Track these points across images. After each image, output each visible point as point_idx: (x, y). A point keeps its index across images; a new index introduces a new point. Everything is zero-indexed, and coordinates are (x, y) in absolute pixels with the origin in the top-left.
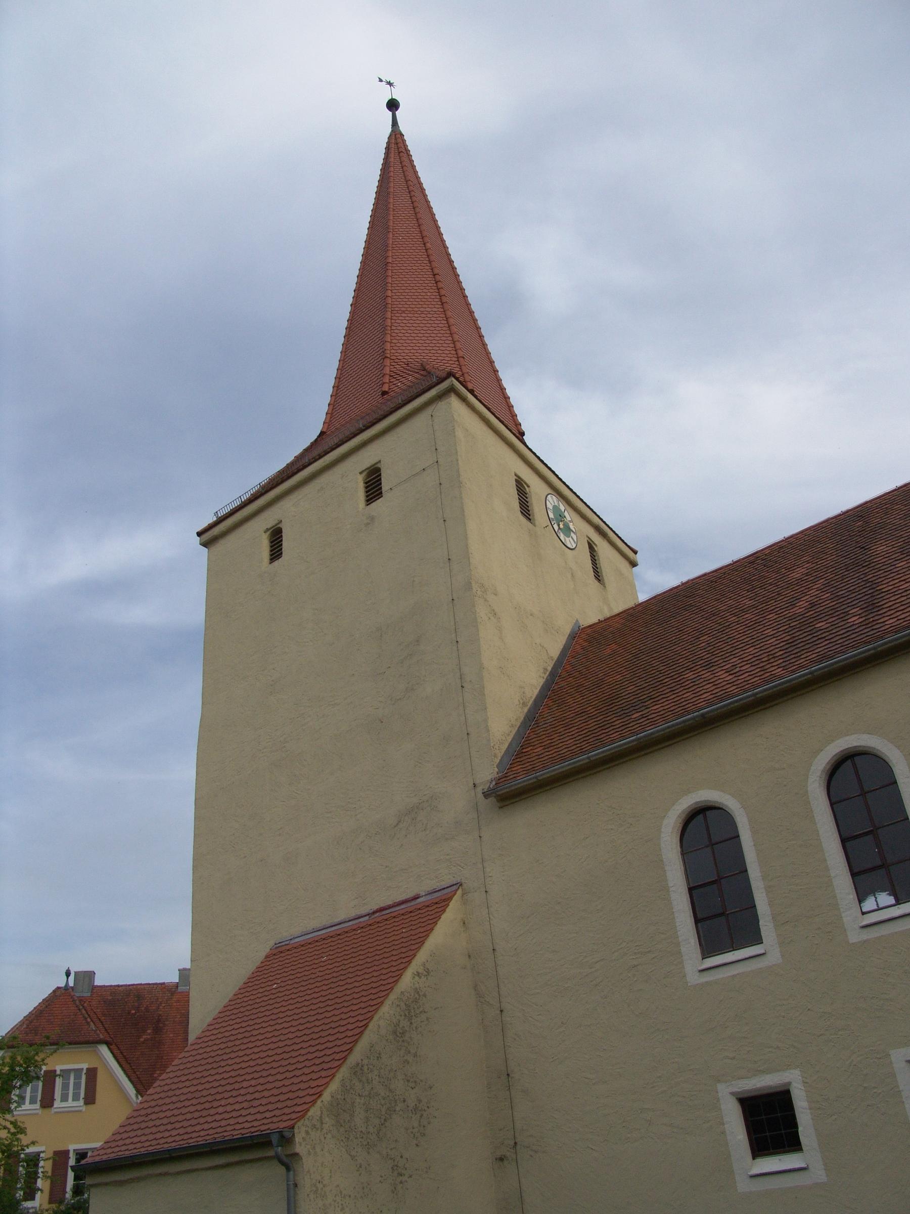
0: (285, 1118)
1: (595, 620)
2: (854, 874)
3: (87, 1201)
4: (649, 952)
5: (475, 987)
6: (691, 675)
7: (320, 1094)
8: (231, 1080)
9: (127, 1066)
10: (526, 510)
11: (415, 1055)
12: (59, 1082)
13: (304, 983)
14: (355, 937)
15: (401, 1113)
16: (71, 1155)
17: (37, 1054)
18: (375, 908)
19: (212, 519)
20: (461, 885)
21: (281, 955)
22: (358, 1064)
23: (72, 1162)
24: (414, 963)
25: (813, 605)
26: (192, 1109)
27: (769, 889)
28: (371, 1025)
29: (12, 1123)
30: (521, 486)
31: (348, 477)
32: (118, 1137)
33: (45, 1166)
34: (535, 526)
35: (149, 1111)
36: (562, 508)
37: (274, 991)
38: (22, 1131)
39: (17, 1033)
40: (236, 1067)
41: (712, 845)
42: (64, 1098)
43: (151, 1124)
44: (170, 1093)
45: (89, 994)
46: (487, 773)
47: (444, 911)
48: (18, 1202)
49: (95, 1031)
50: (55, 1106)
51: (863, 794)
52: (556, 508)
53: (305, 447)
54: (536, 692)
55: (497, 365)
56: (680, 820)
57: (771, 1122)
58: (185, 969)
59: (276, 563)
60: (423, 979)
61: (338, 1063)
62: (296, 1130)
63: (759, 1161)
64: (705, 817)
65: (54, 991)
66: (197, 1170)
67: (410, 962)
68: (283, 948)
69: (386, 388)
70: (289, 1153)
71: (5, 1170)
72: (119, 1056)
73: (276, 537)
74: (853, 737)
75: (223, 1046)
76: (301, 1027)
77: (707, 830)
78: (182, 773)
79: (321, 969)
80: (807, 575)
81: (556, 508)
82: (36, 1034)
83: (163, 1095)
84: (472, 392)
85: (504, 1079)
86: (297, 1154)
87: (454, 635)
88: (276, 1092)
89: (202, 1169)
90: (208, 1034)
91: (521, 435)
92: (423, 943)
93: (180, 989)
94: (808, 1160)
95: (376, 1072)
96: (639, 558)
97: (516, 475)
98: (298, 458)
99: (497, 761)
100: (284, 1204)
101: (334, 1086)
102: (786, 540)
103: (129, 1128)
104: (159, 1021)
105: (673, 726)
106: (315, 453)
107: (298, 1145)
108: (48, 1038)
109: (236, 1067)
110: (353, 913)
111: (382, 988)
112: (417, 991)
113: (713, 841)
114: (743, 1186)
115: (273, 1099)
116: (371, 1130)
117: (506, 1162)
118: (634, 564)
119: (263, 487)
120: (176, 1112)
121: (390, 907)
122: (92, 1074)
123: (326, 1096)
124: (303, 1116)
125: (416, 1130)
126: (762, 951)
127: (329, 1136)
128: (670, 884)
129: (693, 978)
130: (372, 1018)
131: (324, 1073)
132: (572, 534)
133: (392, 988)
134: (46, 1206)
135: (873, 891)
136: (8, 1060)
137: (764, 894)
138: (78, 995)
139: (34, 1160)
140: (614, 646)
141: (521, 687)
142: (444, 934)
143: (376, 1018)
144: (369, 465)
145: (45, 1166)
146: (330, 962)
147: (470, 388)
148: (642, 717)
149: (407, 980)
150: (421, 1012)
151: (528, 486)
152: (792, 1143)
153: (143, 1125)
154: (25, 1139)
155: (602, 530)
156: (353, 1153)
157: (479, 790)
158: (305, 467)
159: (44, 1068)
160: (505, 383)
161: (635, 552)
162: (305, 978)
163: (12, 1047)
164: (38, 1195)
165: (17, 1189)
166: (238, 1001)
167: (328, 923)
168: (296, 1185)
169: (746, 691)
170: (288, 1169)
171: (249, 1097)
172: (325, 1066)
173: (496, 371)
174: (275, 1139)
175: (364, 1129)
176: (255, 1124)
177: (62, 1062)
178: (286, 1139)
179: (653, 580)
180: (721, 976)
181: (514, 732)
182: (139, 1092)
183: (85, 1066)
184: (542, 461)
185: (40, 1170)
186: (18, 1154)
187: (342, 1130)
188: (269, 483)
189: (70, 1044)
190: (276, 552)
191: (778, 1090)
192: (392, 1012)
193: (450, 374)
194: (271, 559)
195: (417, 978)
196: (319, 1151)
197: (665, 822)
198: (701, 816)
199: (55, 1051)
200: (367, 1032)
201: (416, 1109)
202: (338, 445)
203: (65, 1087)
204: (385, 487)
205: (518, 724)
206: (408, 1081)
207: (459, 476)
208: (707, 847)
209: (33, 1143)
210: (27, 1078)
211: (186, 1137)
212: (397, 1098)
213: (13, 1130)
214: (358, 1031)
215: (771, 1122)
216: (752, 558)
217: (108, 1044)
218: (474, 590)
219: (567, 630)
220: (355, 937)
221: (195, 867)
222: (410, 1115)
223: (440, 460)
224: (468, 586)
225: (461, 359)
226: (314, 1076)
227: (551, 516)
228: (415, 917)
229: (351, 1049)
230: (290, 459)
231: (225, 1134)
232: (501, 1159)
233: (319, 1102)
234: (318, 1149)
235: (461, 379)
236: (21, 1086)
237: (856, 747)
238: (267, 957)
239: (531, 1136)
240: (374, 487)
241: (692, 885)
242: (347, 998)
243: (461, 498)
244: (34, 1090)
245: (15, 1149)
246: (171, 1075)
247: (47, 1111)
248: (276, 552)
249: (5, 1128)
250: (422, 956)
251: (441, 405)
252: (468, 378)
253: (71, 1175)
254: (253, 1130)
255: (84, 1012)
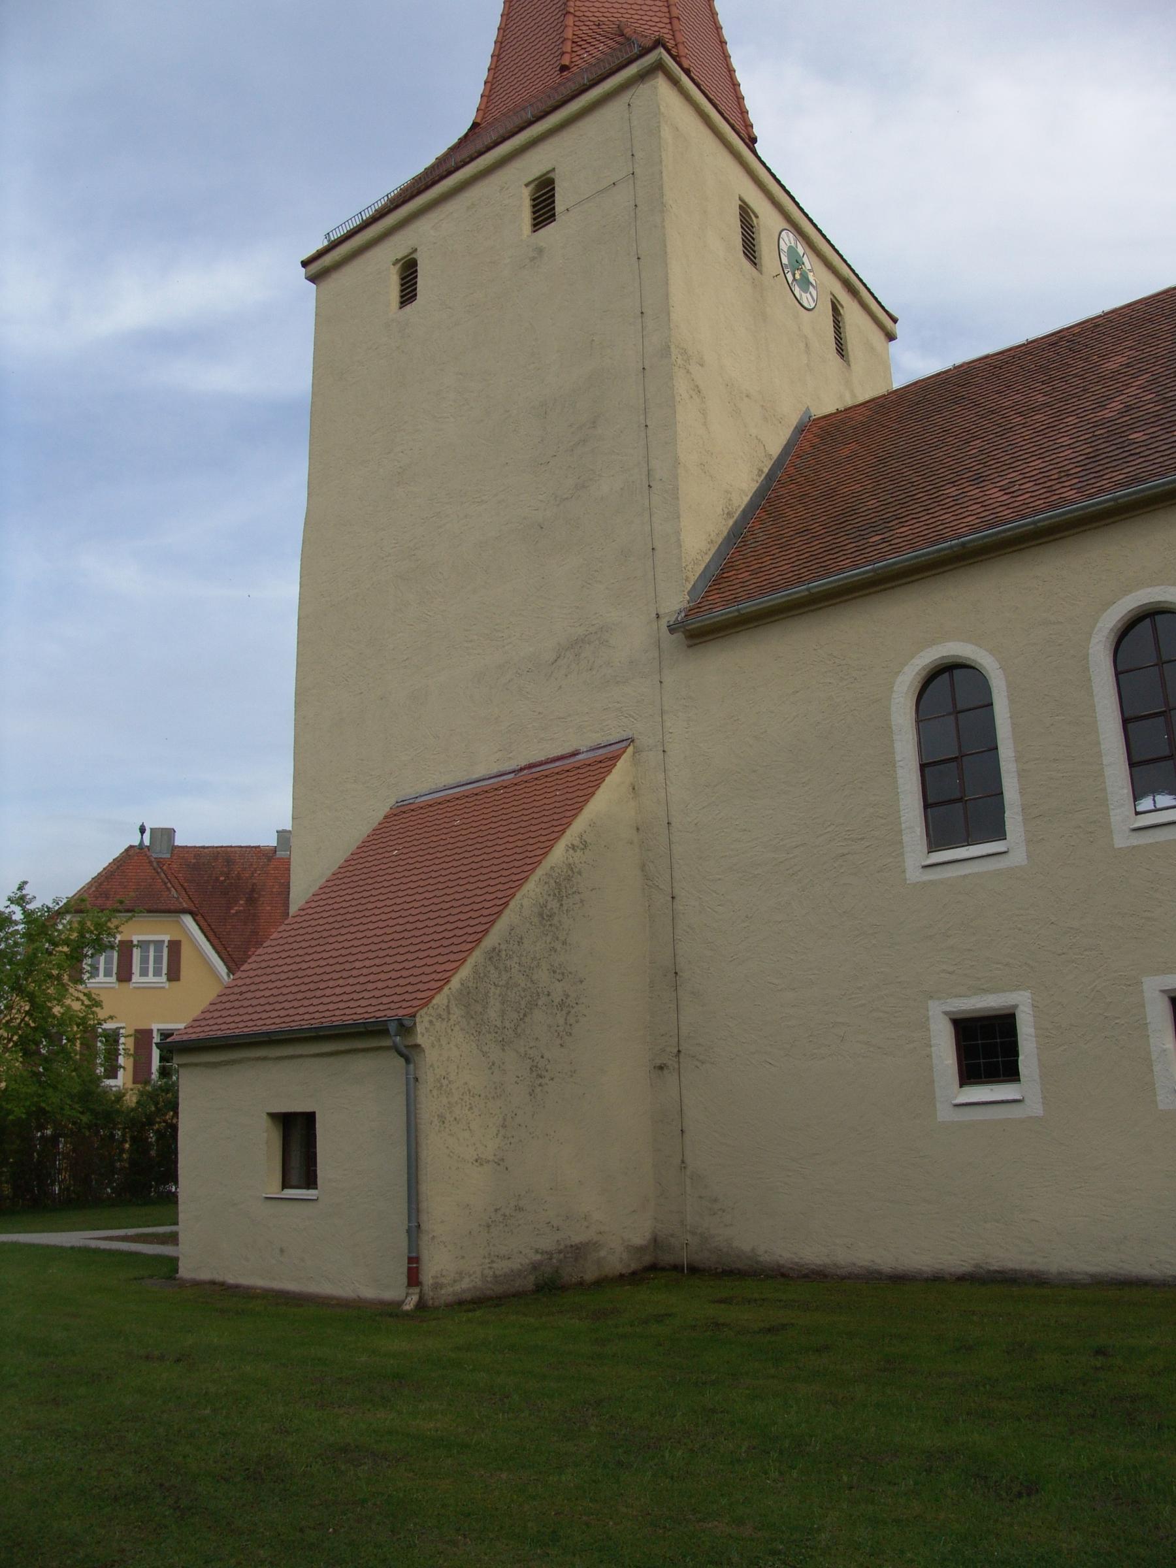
0: (405, 1004)
1: (831, 409)
2: (1132, 765)
3: (176, 1084)
4: (862, 839)
5: (643, 867)
6: (953, 491)
7: (447, 981)
8: (341, 960)
9: (216, 942)
10: (750, 250)
11: (564, 943)
12: (136, 953)
13: (431, 851)
14: (497, 798)
15: (544, 1008)
16: (155, 1034)
17: (110, 920)
18: (523, 764)
19: (322, 244)
20: (633, 741)
21: (404, 816)
22: (494, 949)
23: (156, 1039)
24: (568, 833)
25: (1129, 408)
26: (294, 989)
27: (1021, 774)
28: (512, 904)
29: (85, 994)
30: (746, 215)
31: (510, 190)
32: (208, 1015)
33: (126, 1043)
34: (761, 272)
35: (244, 989)
36: (800, 250)
37: (394, 859)
38: (98, 1004)
39: (86, 896)
40: (347, 944)
41: (957, 712)
42: (144, 972)
43: (246, 1003)
44: (269, 971)
45: (168, 856)
46: (675, 601)
47: (610, 771)
48: (99, 1078)
49: (177, 899)
50: (134, 980)
51: (1161, 663)
52: (792, 251)
53: (450, 145)
54: (746, 499)
55: (727, 34)
56: (919, 678)
57: (987, 1048)
58: (284, 831)
59: (408, 308)
60: (579, 853)
61: (469, 946)
62: (418, 1019)
63: (966, 1089)
64: (952, 677)
65: (127, 850)
66: (301, 1056)
67: (563, 831)
68: (406, 808)
69: (566, 60)
70: (407, 1043)
71: (81, 1044)
72: (207, 929)
73: (409, 271)
74: (1157, 589)
75: (331, 920)
76: (426, 902)
77: (953, 699)
78: (282, 590)
79: (453, 835)
80: (1128, 365)
81: (792, 251)
82: (107, 898)
83: (259, 972)
84: (687, 72)
85: (670, 977)
86: (417, 1046)
87: (642, 417)
88: (394, 975)
89: (307, 1056)
90: (313, 905)
91: (751, 141)
92: (581, 809)
93: (279, 854)
94: (1025, 1094)
95: (516, 959)
96: (898, 329)
97: (741, 199)
98: (441, 161)
99: (689, 586)
100: (401, 1100)
101: (465, 972)
102: (1105, 315)
103: (218, 1007)
104: (253, 890)
105: (923, 555)
106: (464, 154)
107: (419, 1036)
108: (121, 902)
109: (347, 944)
110: (495, 770)
111: (528, 861)
112: (570, 867)
113: (960, 707)
114: (944, 1114)
115: (391, 983)
116: (507, 1024)
117: (666, 1071)
118: (891, 337)
119: (391, 201)
120: (275, 992)
121: (541, 764)
122: (175, 947)
123: (455, 983)
124: (426, 1004)
125: (561, 1028)
126: (1003, 849)
127: (457, 1028)
128: (898, 758)
129: (914, 875)
130: (513, 895)
131: (452, 957)
132: (811, 289)
133: (540, 862)
134: (130, 1085)
135: (1154, 791)
136: (76, 925)
137: (1016, 780)
138: (155, 855)
139: (112, 1038)
140: (854, 446)
141: (727, 492)
142: (607, 800)
143: (518, 896)
144: (538, 174)
145: (126, 1043)
146: (464, 827)
147: (686, 66)
148: (884, 541)
149: (559, 853)
150: (574, 893)
151: (757, 217)
152: (1009, 1071)
153: (237, 1004)
154: (102, 1014)
155: (852, 285)
156: (485, 1049)
157: (664, 623)
158: (450, 173)
159: (119, 938)
160: (735, 62)
161: (895, 321)
162: (432, 845)
163: (81, 911)
164: (121, 1073)
165: (99, 1078)
166: (351, 868)
167: (464, 779)
168: (416, 1080)
169: (1023, 517)
170: (408, 1060)
171: (362, 979)
172: (454, 948)
173: (723, 43)
174: (392, 1027)
175: (498, 1023)
176: (370, 1009)
177: (140, 931)
178: (405, 1028)
179: (912, 362)
180: (949, 875)
181: (713, 551)
182: (231, 971)
183: (166, 938)
184: (778, 182)
185: (121, 1047)
186: (94, 1028)
187: (472, 1022)
188: (399, 195)
189: (149, 911)
190: (408, 294)
191: (1002, 1012)
192: (538, 890)
193: (659, 43)
194: (402, 303)
195: (571, 851)
196: (444, 1043)
197: (900, 679)
198: (946, 675)
199: (131, 918)
200: (507, 912)
201: (562, 1005)
202: (496, 144)
203: (144, 960)
204: (559, 206)
205: (720, 540)
206: (554, 972)
207: (662, 195)
208: (950, 714)
209: (111, 1017)
210: (100, 947)
211: (287, 1019)
212: (540, 990)
213: (87, 1002)
214: (497, 909)
215: (987, 1048)
216: (1054, 338)
217: (191, 913)
218: (674, 357)
219: (793, 420)
220: (497, 798)
221: (297, 705)
222: (555, 1011)
223: (637, 171)
224: (665, 352)
225: (675, 21)
226: (441, 959)
227: (785, 260)
228: (571, 778)
229: (486, 931)
230: (430, 161)
231: (334, 1019)
232: (661, 1068)
233: (446, 989)
234: (444, 1042)
235: (674, 51)
236: (92, 956)
237: (1160, 602)
238: (386, 817)
239: (699, 1044)
240: (544, 207)
241: (925, 761)
242: (484, 871)
243: (664, 227)
244: (108, 962)
245: (91, 1022)
246: (270, 950)
247: (124, 985)
248: (408, 294)
249: (78, 999)
250: (579, 825)
251: (643, 89)
252: (683, 50)
253: (156, 1053)
254: (366, 1016)
255: (163, 875)
